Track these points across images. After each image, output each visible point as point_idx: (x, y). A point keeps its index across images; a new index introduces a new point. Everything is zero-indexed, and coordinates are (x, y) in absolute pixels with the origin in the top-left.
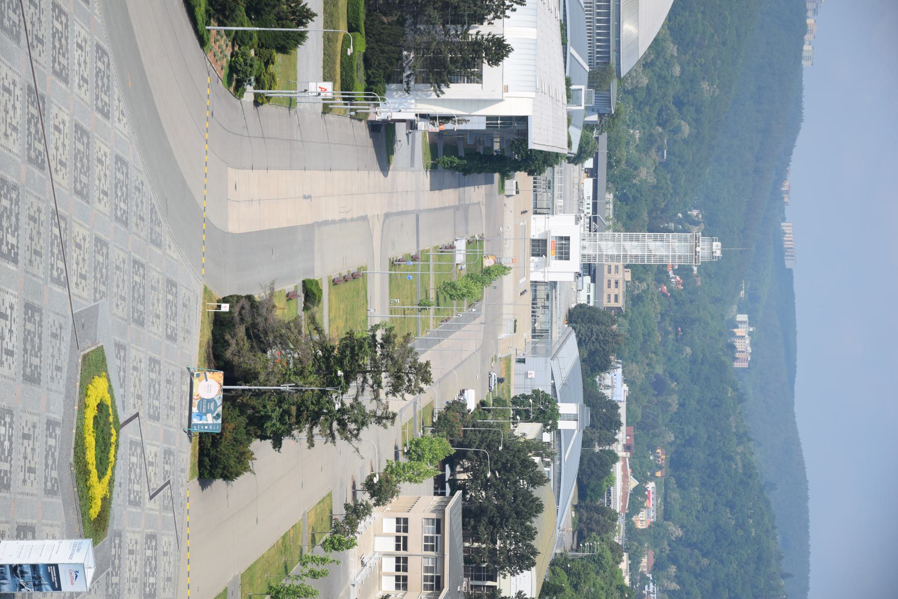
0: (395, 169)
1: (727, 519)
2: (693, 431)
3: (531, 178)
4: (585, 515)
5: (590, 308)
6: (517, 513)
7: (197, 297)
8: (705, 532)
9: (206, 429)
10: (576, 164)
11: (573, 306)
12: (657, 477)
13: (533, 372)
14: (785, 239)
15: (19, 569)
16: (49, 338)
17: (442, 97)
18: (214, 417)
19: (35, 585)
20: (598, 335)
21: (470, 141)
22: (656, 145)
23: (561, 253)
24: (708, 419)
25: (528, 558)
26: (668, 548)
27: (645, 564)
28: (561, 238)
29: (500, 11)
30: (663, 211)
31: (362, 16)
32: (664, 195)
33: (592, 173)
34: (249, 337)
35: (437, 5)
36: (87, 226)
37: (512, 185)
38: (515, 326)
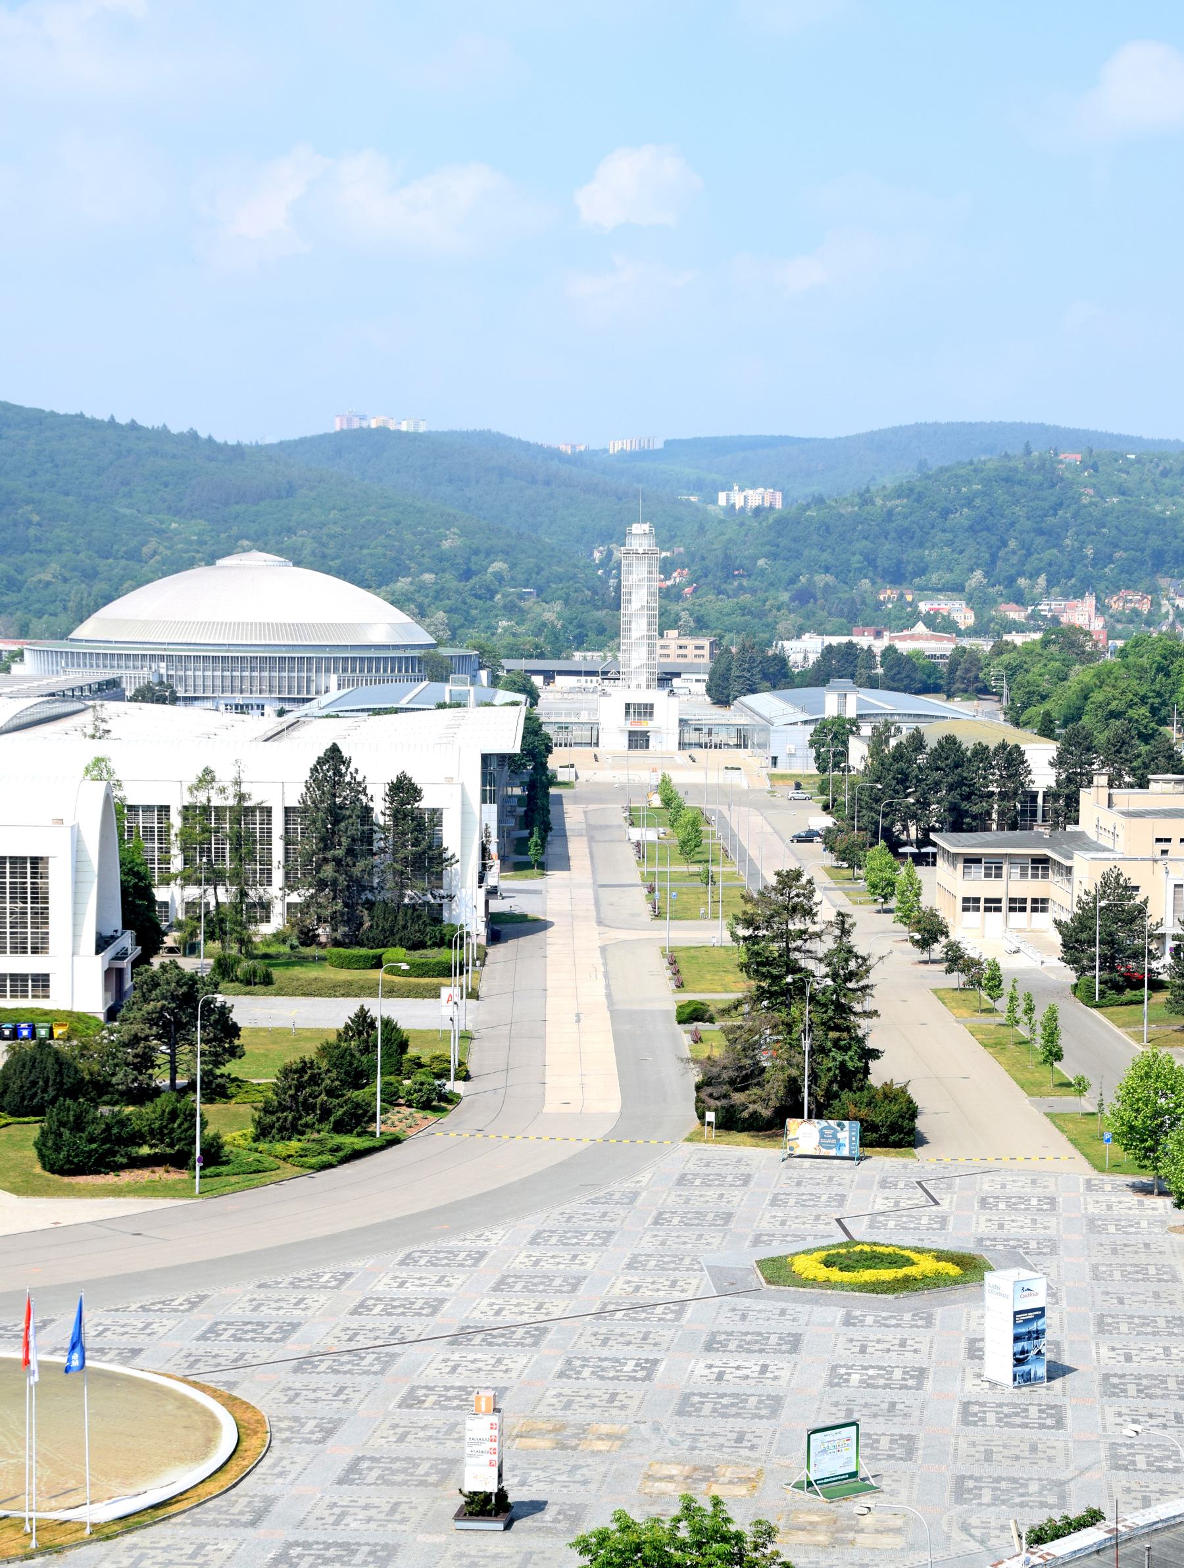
2: (858, 557)
3: (555, 749)
5: (711, 679)
6: (957, 766)
11: (708, 699)
16: (747, 1323)
17: (458, 857)
19: (1037, 1338)
20: (744, 670)
21: (512, 823)
23: (645, 713)
25: (1010, 753)
28: (627, 713)
29: (359, 788)
30: (595, 593)
31: (363, 951)
32: (576, 591)
33: (549, 676)
35: (350, 863)
38: (732, 768)
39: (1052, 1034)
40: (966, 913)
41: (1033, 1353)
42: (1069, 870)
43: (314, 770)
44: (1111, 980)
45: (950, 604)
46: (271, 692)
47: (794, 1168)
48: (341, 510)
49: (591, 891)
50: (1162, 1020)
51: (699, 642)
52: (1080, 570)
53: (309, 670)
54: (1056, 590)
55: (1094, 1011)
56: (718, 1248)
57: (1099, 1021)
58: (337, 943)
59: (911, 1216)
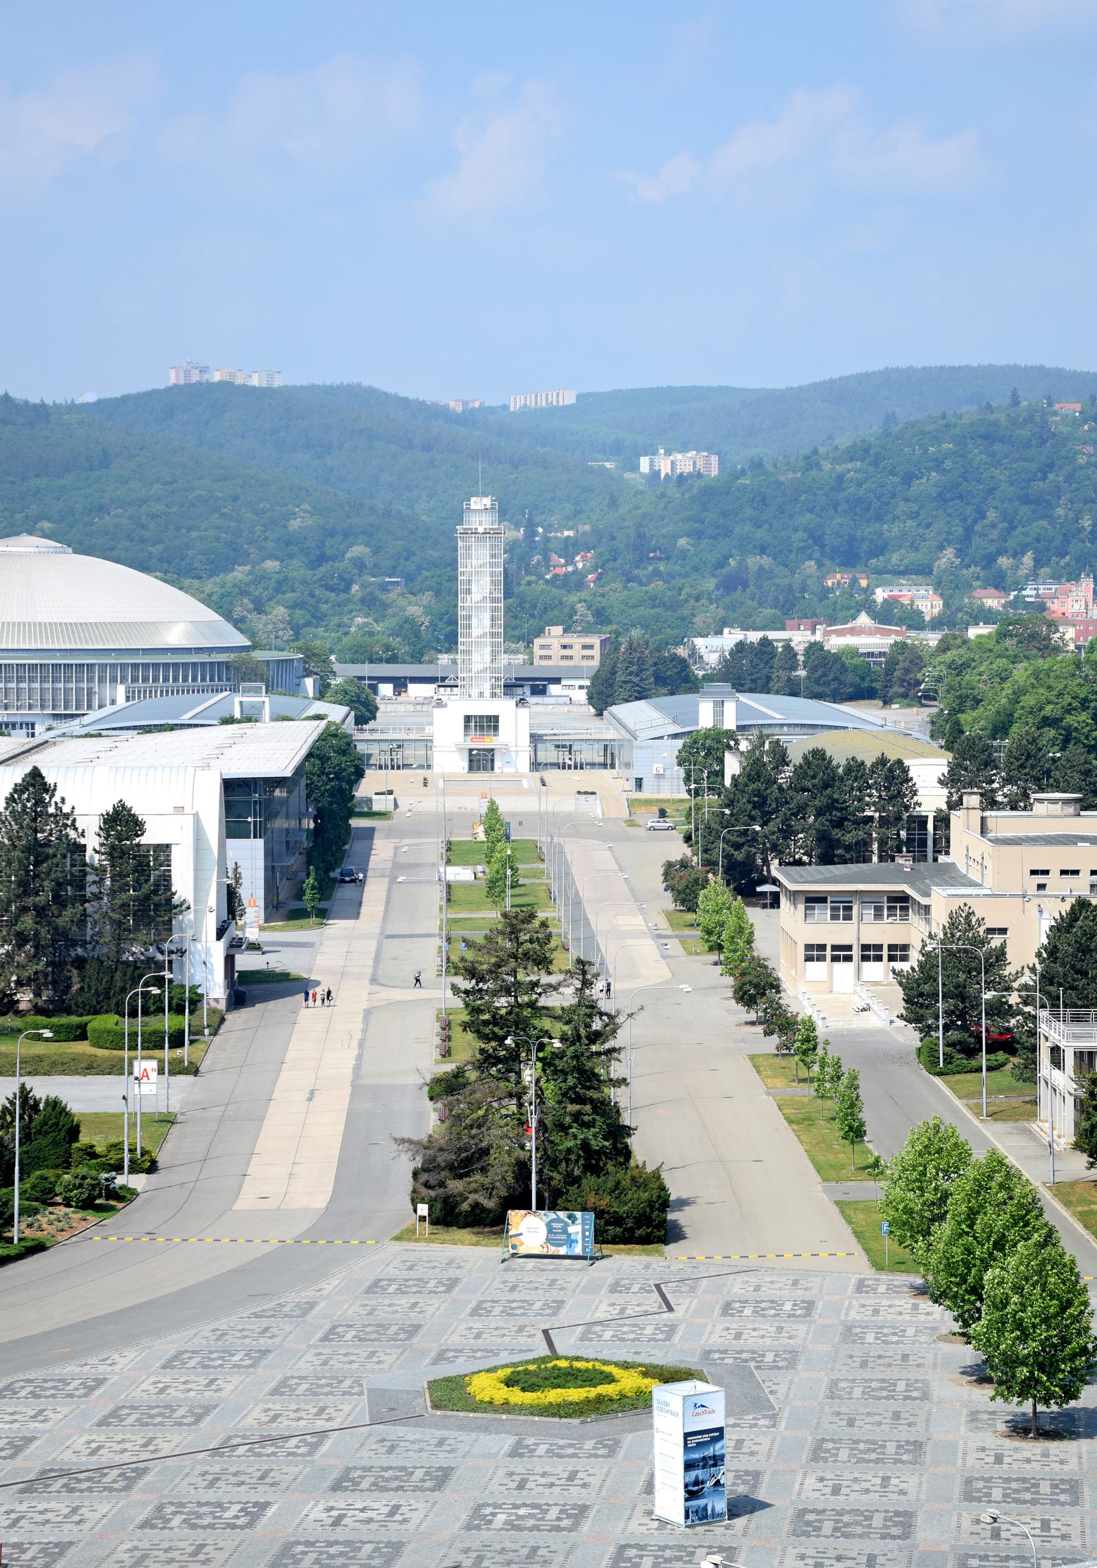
0: (310, 971)
1: (930, 483)
2: (800, 534)
4: (896, 689)
6: (826, 786)
7: (406, 1250)
8: (949, 515)
9: (590, 1234)
10: (377, 709)
12: (868, 585)
13: (655, 766)
14: (533, 405)
15: (691, 1488)
16: (393, 1456)
18: (573, 1222)
19: (715, 1465)
20: (631, 674)
22: (378, 593)
24: (783, 513)
25: (890, 770)
26: (973, 569)
27: (996, 601)
28: (467, 727)
29: (65, 819)
33: (400, 684)
34: (467, 1175)
35: (56, 912)
36: (251, 1406)
37: (380, 800)
38: (586, 793)
39: (852, 1106)
40: (808, 963)
41: (709, 1484)
42: (927, 909)
43: (10, 800)
44: (960, 1042)
45: (914, 589)
46: (43, 707)
47: (514, 1270)
48: (167, 483)
49: (374, 943)
50: (1013, 1089)
51: (588, 640)
52: (1074, 547)
53: (90, 680)
54: (1045, 571)
55: (937, 1080)
56: (390, 1367)
57: (939, 1091)
58: (38, 1010)
59: (634, 1325)
